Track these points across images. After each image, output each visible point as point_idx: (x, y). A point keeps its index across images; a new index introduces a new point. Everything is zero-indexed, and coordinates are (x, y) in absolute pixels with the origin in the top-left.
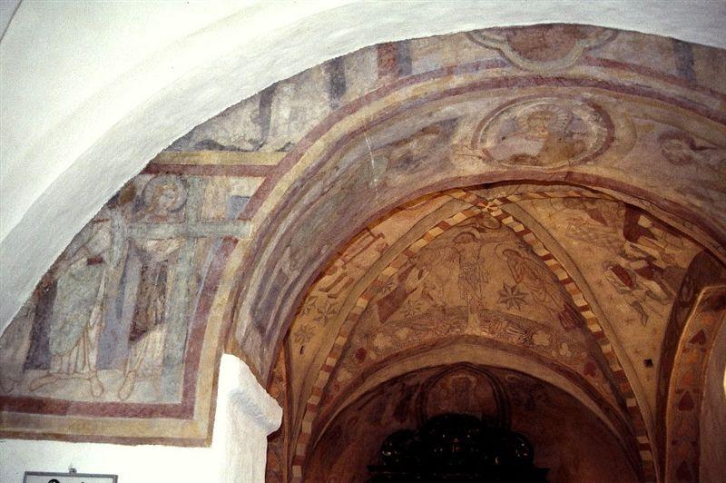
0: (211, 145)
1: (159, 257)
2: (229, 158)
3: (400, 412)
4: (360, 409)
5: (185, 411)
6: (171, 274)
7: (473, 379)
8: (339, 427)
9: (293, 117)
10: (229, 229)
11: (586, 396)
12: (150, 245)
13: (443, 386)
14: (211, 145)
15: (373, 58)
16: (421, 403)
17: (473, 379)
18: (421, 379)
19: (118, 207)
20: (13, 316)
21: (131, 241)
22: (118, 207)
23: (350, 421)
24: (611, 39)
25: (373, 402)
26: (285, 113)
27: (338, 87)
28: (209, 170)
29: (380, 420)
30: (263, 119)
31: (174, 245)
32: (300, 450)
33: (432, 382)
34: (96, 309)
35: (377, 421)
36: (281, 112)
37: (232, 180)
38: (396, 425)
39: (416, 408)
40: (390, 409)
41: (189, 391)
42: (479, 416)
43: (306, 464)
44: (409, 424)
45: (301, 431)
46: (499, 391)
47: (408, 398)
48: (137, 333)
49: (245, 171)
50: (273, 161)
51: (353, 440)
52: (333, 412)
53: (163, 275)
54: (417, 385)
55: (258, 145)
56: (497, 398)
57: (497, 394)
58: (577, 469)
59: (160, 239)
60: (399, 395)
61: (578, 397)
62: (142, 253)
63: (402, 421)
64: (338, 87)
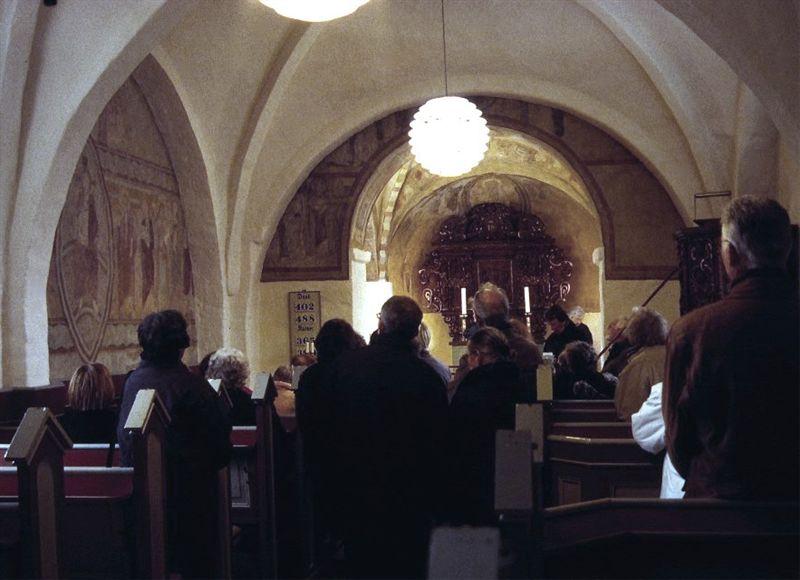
0: (332, 164)
1: (320, 213)
2: (341, 170)
3: (451, 203)
5: (339, 268)
6: (326, 219)
7: (499, 181)
9: (364, 149)
10: (345, 200)
12: (317, 208)
13: (480, 187)
14: (332, 164)
15: (394, 118)
17: (499, 181)
18: (464, 183)
21: (309, 206)
24: (494, 102)
25: (432, 201)
26: (360, 148)
27: (380, 136)
28: (334, 176)
30: (352, 152)
31: (325, 207)
32: (384, 241)
33: (471, 185)
34: (301, 235)
35: (436, 211)
36: (359, 148)
37: (343, 179)
38: (449, 213)
40: (443, 203)
41: (339, 263)
42: (508, 203)
43: (388, 249)
47: (456, 195)
48: (318, 242)
49: (348, 175)
50: (359, 170)
53: (323, 220)
54: (460, 188)
55: (352, 163)
59: (320, 205)
62: (314, 211)
64: (380, 136)
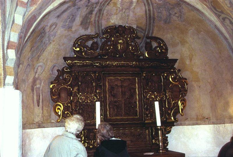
3: (85, 23)
4: (58, 16)
8: (44, 29)
11: (209, 11)
16: (99, 17)
19: (66, 18)
20: (1, 42)
22: (66, 18)
23: (51, 26)
29: (71, 27)
32: (14, 37)
35: (70, 28)
39: (95, 20)
40: (78, 20)
44: (90, 31)
45: (13, 21)
46: (149, 10)
47: (91, 12)
51: (54, 41)
52: (40, 14)
56: (148, 15)
57: (148, 12)
58: (191, 60)
60: (85, 10)
61: (203, 11)
63: (86, 29)
